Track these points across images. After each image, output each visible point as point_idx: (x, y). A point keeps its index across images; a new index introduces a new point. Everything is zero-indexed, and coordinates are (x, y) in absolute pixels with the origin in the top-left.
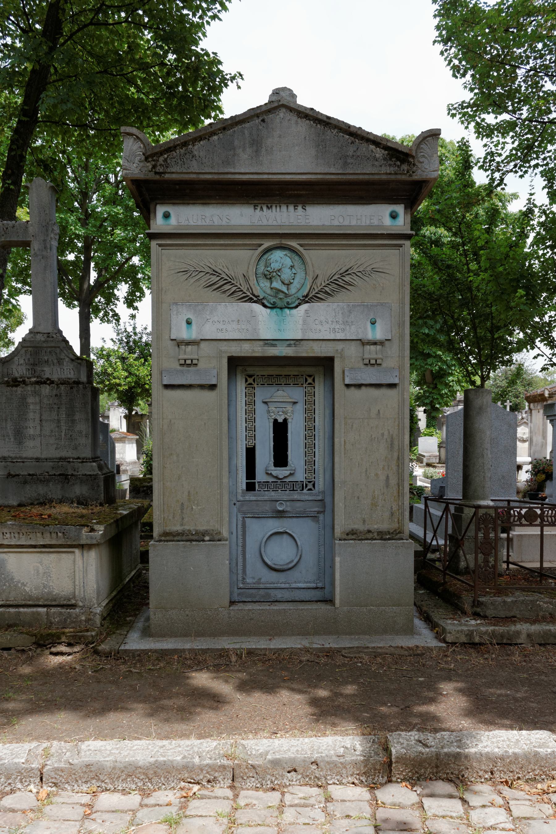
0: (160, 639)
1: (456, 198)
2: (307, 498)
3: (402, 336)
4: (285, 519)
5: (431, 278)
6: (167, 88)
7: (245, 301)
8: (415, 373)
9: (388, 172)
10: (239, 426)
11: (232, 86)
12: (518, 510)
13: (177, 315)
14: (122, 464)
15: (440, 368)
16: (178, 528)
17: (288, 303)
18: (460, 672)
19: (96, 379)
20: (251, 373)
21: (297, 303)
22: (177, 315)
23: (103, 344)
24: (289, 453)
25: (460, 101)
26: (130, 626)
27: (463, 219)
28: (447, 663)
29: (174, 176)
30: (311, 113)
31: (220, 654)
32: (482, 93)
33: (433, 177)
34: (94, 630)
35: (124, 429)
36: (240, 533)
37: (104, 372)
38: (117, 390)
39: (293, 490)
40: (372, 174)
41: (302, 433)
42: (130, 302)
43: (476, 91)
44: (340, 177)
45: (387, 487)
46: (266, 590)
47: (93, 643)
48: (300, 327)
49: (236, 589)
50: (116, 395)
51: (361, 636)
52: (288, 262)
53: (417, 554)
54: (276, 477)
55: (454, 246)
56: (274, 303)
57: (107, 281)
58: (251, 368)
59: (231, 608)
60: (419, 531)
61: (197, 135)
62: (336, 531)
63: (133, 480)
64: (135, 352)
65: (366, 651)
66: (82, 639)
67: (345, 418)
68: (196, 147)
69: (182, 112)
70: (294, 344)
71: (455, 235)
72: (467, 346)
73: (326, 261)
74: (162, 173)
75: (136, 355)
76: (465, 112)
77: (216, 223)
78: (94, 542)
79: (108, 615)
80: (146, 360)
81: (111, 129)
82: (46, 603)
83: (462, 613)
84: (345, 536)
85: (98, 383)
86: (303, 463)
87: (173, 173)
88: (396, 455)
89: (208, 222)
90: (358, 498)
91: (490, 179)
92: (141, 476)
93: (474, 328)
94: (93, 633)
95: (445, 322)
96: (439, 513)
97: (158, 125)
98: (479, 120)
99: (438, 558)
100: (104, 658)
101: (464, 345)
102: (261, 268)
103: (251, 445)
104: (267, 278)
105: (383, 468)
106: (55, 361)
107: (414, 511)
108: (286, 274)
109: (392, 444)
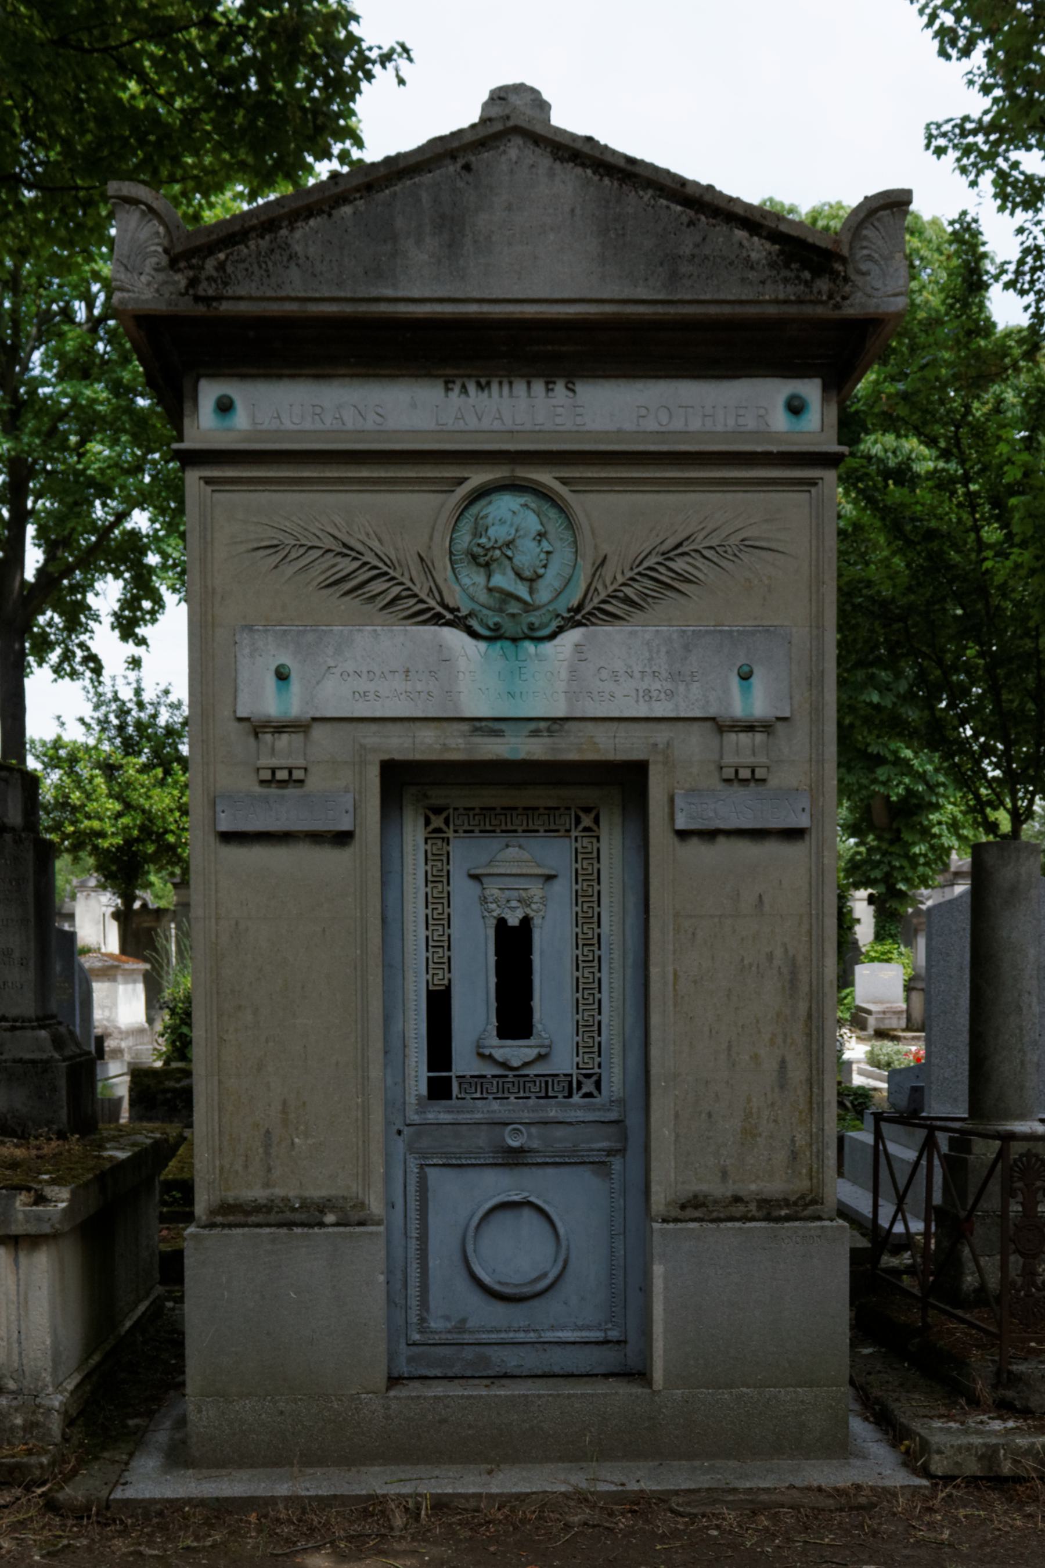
0: (214, 1472)
1: (949, 364)
3: (817, 710)
4: (526, 1170)
5: (886, 563)
6: (219, 83)
7: (424, 623)
8: (846, 804)
9: (781, 296)
10: (409, 937)
11: (383, 76)
13: (252, 656)
14: (109, 1035)
15: (907, 789)
16: (257, 1193)
17: (531, 627)
18: (965, 1548)
19: (45, 820)
20: (440, 802)
22: (252, 656)
23: (59, 730)
24: (536, 1003)
25: (958, 115)
26: (137, 1440)
27: (964, 416)
28: (931, 1526)
29: (243, 307)
30: (586, 149)
31: (365, 1509)
32: (1013, 97)
33: (892, 309)
34: (46, 1452)
35: (113, 945)
36: (413, 1205)
37: (63, 804)
38: (96, 848)
39: (547, 1097)
40: (741, 302)
41: (568, 953)
42: (127, 626)
43: (998, 92)
44: (660, 309)
46: (477, 1349)
47: (43, 1483)
50: (91, 861)
51: (719, 1463)
52: (532, 523)
53: (856, 1255)
54: (504, 1065)
55: (943, 483)
56: (497, 627)
57: (68, 571)
58: (438, 789)
59: (392, 1393)
60: (860, 1200)
61: (301, 203)
62: (654, 1198)
63: (139, 1075)
64: (139, 753)
65: (731, 1498)
66: (16, 1474)
67: (677, 915)
68: (298, 234)
69: (259, 147)
70: (549, 730)
71: (945, 455)
72: (976, 736)
73: (624, 520)
75: (143, 759)
76: (973, 145)
77: (350, 426)
78: (46, 1229)
79: (81, 1413)
80: (167, 772)
81: (77, 188)
83: (969, 1402)
84: (676, 1213)
85: (49, 830)
86: (570, 1028)
88: (803, 1007)
89: (329, 422)
90: (710, 1115)
91: (1034, 315)
92: (159, 1064)
93: (994, 690)
94: (44, 1460)
95: (922, 677)
96: (911, 1155)
97: (196, 178)
98: (1005, 166)
99: (908, 1266)
100: (70, 1522)
101: (969, 733)
102: (464, 539)
103: (439, 982)
104: (479, 565)
105: (772, 1042)
107: (847, 1149)
108: (527, 554)
109: (793, 982)
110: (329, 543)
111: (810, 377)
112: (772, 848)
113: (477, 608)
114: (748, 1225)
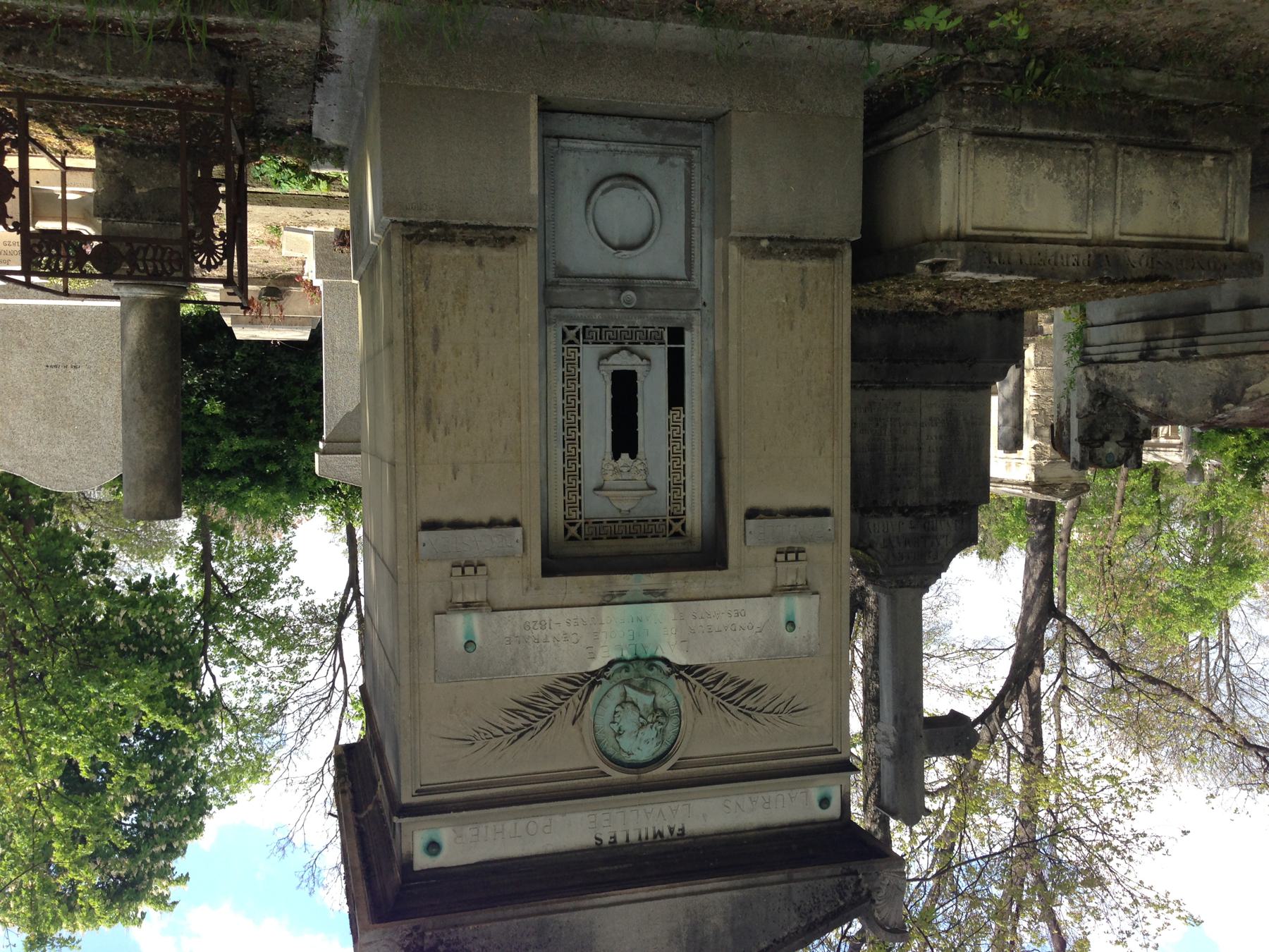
2: (579, 313)
4: (616, 274)
7: (698, 667)
12: (136, 273)
16: (811, 264)
21: (611, 671)
22: (810, 637)
33: (372, 933)
36: (696, 251)
39: (601, 327)
40: (490, 921)
44: (550, 907)
45: (436, 330)
46: (652, 140)
48: (604, 628)
49: (704, 145)
52: (626, 743)
54: (632, 352)
56: (650, 667)
68: (795, 924)
73: (562, 750)
74: (846, 874)
77: (746, 797)
78: (944, 245)
82: (1020, 141)
84: (518, 235)
87: (830, 877)
88: (421, 392)
90: (492, 310)
102: (671, 728)
104: (661, 710)
106: (895, 544)
108: (629, 720)
110: (760, 717)
111: (423, 871)
112: (446, 515)
113: (664, 680)
114: (463, 222)
